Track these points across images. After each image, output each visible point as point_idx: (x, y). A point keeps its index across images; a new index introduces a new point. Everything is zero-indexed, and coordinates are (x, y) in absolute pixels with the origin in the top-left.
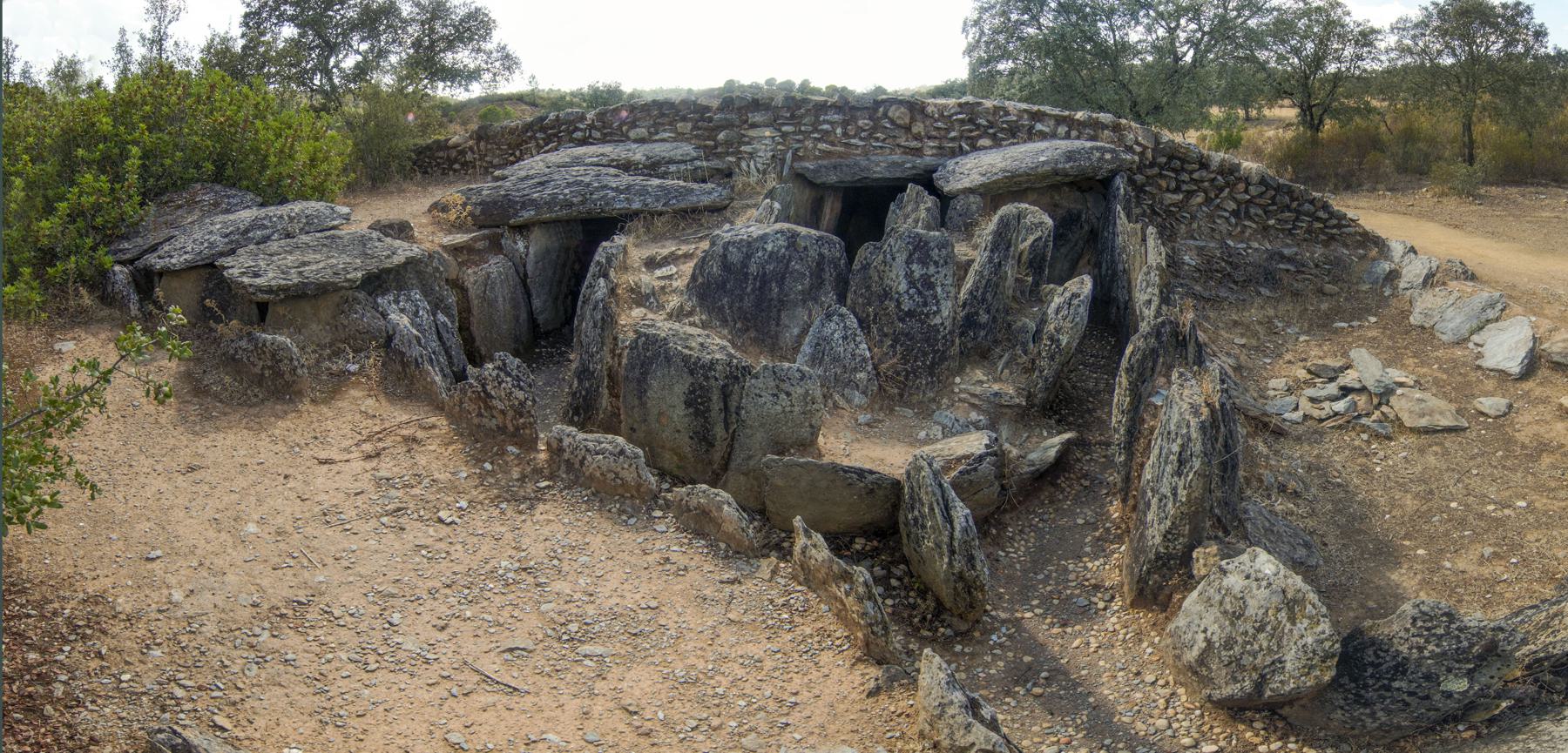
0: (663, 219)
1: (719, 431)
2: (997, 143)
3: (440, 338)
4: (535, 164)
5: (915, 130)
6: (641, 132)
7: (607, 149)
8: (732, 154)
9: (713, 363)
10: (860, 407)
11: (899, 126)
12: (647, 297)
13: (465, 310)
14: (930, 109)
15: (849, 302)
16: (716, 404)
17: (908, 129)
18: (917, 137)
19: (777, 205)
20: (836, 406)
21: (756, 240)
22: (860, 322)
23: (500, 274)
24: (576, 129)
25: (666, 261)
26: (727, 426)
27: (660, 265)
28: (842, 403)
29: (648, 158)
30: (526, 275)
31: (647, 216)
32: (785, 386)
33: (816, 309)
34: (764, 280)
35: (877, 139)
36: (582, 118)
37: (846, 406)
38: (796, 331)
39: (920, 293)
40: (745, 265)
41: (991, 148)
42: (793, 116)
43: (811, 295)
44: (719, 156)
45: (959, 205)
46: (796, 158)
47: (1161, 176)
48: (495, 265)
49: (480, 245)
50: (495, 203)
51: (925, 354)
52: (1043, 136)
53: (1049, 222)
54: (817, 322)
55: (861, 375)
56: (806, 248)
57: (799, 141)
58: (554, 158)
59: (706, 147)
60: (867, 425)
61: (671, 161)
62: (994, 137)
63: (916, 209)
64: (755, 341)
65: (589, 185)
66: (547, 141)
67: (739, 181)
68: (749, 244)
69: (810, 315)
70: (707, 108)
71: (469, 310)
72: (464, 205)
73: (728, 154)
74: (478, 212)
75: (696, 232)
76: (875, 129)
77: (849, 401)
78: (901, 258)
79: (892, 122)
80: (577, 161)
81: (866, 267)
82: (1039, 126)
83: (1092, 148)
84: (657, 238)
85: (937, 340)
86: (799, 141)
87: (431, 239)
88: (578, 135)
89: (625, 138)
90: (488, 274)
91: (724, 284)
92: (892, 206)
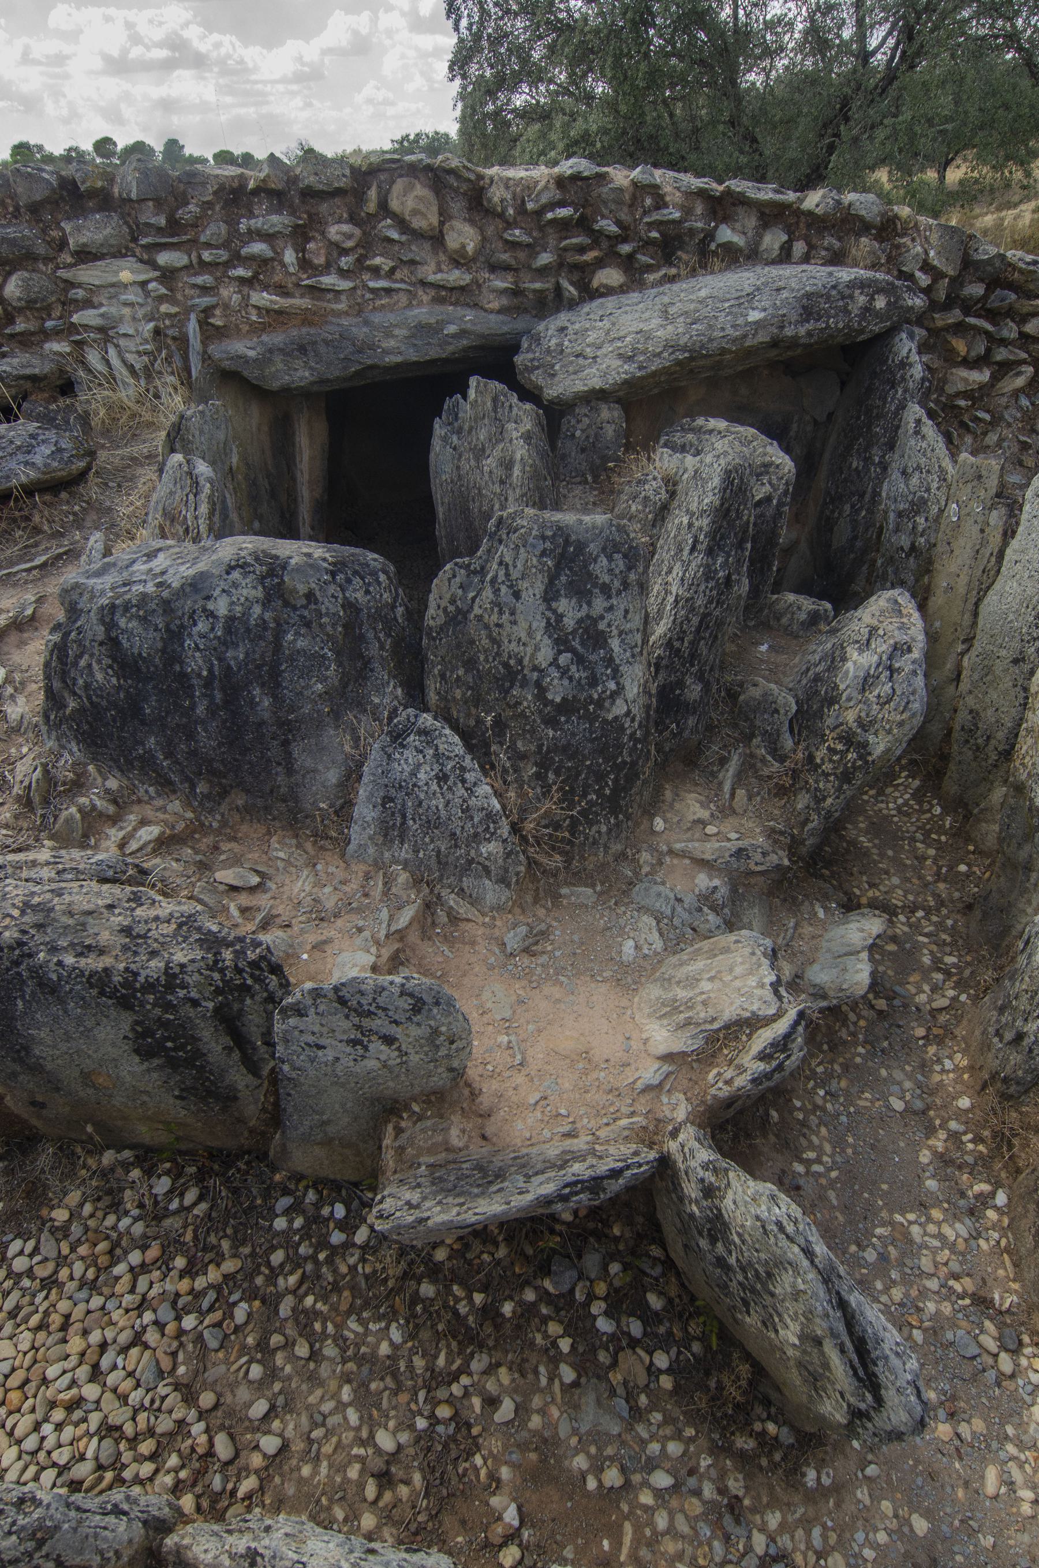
1: (239, 1078)
2: (635, 277)
5: (452, 242)
8: (56, 334)
9: (172, 978)
10: (499, 908)
11: (417, 235)
14: (497, 194)
15: (432, 697)
16: (213, 1043)
17: (437, 239)
18: (459, 259)
19: (202, 468)
20: (454, 919)
21: (181, 593)
22: (466, 736)
26: (252, 1066)
28: (463, 909)
32: (378, 1023)
33: (365, 725)
34: (230, 687)
35: (376, 271)
37: (472, 913)
38: (332, 776)
39: (580, 660)
41: (622, 290)
42: (174, 226)
43: (348, 696)
45: (579, 426)
46: (211, 333)
47: (960, 328)
51: (601, 777)
52: (733, 257)
53: (785, 463)
54: (375, 755)
55: (491, 848)
56: (310, 596)
57: (205, 290)
60: (526, 950)
62: (628, 264)
63: (499, 435)
64: (248, 812)
67: (94, 400)
68: (167, 606)
69: (356, 740)
73: (47, 335)
75: (26, 554)
76: (367, 245)
77: (475, 902)
78: (533, 590)
79: (402, 224)
81: (458, 617)
82: (726, 234)
83: (852, 285)
85: (620, 746)
86: (205, 290)
92: (439, 429)
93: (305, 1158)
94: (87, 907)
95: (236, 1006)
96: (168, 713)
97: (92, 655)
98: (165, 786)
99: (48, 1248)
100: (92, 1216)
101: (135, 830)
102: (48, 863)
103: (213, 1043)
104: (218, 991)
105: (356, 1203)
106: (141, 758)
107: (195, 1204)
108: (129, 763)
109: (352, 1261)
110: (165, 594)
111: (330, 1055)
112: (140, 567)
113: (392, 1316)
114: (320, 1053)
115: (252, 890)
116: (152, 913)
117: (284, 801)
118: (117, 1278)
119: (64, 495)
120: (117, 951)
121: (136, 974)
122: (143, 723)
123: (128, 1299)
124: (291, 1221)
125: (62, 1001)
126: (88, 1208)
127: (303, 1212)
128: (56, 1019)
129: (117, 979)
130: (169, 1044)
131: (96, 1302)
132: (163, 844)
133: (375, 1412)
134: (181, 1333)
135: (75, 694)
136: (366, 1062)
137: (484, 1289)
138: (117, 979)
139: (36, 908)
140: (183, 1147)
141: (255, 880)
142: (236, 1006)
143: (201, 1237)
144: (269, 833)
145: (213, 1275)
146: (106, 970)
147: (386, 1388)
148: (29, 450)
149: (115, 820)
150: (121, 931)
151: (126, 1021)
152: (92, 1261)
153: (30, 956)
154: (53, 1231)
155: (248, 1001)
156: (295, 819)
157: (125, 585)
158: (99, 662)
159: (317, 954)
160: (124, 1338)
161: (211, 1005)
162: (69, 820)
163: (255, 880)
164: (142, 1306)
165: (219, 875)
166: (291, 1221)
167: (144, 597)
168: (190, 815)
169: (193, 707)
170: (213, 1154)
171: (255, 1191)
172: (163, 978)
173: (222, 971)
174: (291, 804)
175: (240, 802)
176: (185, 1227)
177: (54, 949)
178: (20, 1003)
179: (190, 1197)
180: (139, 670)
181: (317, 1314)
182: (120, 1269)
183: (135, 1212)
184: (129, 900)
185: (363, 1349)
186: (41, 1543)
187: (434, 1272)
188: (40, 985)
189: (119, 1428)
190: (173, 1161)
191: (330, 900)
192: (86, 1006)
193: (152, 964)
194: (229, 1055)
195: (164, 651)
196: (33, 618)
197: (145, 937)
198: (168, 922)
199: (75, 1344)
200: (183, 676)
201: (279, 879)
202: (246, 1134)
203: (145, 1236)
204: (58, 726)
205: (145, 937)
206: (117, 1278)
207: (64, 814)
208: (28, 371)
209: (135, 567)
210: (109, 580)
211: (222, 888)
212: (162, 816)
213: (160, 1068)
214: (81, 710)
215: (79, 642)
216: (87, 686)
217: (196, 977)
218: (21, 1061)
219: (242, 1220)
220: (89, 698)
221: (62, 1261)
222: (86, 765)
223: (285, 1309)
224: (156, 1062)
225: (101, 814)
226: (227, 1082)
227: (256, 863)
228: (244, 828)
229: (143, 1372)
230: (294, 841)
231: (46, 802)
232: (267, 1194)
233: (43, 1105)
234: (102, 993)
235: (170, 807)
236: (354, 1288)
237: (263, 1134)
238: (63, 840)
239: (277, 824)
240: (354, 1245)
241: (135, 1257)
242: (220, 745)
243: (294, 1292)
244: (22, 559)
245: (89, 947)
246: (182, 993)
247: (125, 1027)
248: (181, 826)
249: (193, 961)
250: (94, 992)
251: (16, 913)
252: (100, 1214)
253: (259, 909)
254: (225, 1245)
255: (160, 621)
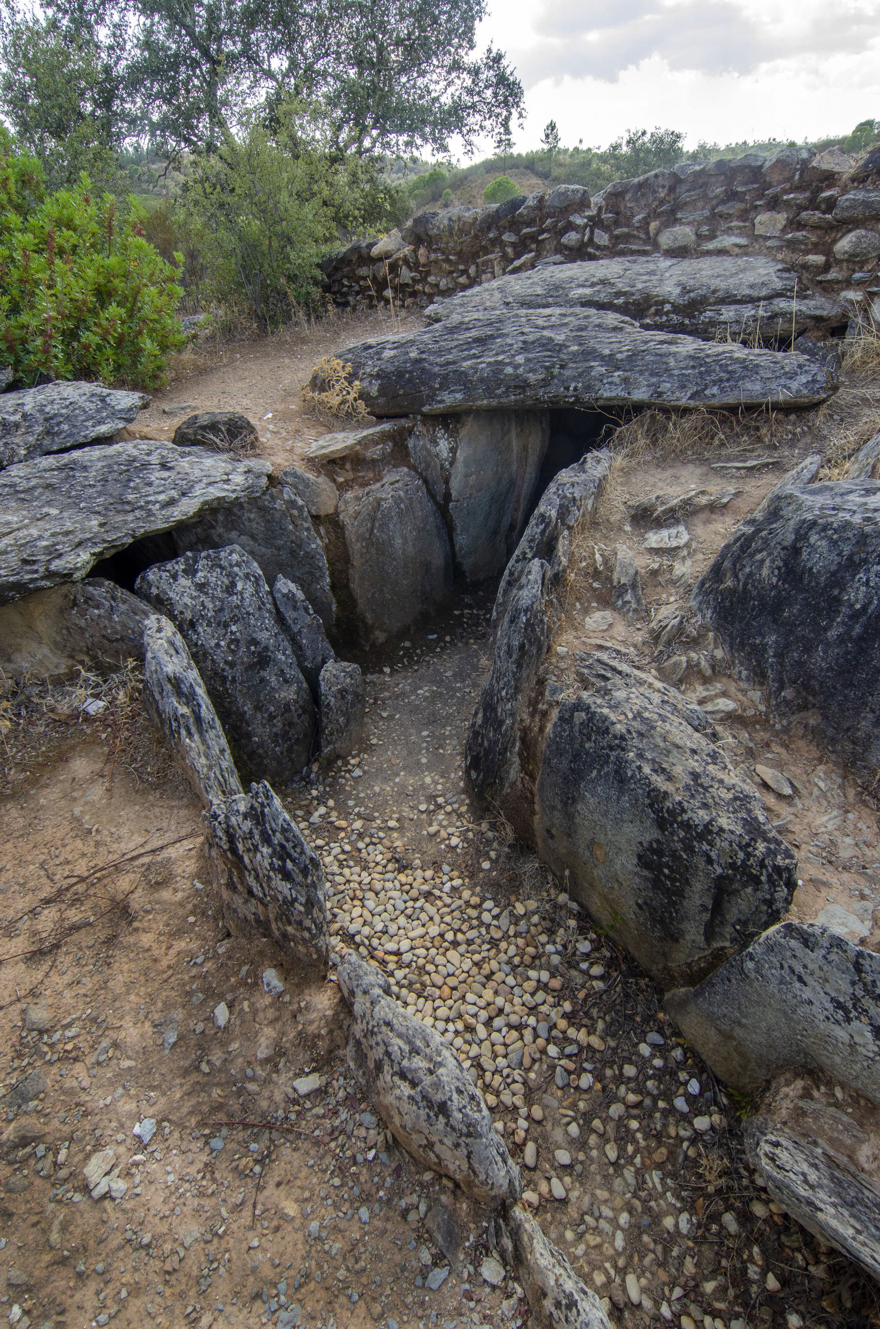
0: (687, 423)
1: (693, 932)
3: (280, 618)
4: (487, 298)
6: (683, 233)
7: (608, 268)
9: (708, 832)
12: (622, 590)
13: (340, 558)
16: (698, 895)
23: (398, 501)
24: (571, 227)
25: (672, 517)
27: (659, 524)
29: (685, 290)
30: (448, 496)
31: (657, 414)
36: (583, 204)
40: (838, 579)
44: (829, 288)
48: (392, 486)
49: (374, 452)
50: (400, 374)
58: (519, 285)
59: (805, 267)
61: (729, 299)
64: (815, 735)
65: (562, 346)
66: (521, 248)
68: (863, 539)
70: (829, 178)
71: (346, 559)
72: (351, 378)
73: (848, 283)
74: (374, 391)
80: (556, 295)
84: (669, 458)
87: (289, 446)
88: (571, 238)
89: (650, 246)
90: (379, 501)
91: (778, 606)
93: (693, 1024)
94: (679, 742)
95: (736, 886)
96: (802, 623)
97: (769, 554)
98: (759, 676)
99: (504, 921)
100: (535, 925)
101: (716, 696)
102: (659, 691)
103: (698, 895)
104: (733, 866)
105: (708, 1095)
106: (754, 646)
107: (596, 978)
108: (742, 645)
109: (682, 1133)
110: (867, 529)
111: (807, 994)
112: (854, 498)
113: (692, 1209)
114: (798, 985)
115: (780, 796)
116: (721, 775)
117: (854, 743)
118: (528, 979)
119: (793, 417)
120: (680, 786)
121: (684, 811)
122: (775, 621)
123: (527, 997)
124: (653, 1056)
125: (621, 792)
126: (535, 919)
127: (666, 1059)
128: (608, 799)
129: (668, 804)
130: (666, 871)
131: (510, 980)
132: (732, 719)
133: (636, 1259)
134: (543, 1052)
135: (736, 576)
136: (836, 1028)
137: (784, 1282)
138: (668, 804)
139: (644, 720)
140: (612, 934)
141: (788, 791)
142: (736, 886)
143: (589, 1004)
144: (820, 761)
145: (582, 1036)
146: (666, 793)
147: (654, 1252)
148: (792, 376)
149: (706, 681)
150: (692, 773)
151: (651, 834)
152: (521, 954)
153: (623, 749)
154: (511, 914)
155: (749, 890)
156: (853, 763)
157: (834, 509)
158: (773, 561)
159: (811, 888)
160: (514, 1019)
161: (719, 871)
162: (676, 665)
163: (788, 791)
164: (533, 1010)
165: (760, 768)
166: (653, 1056)
167: (846, 525)
168: (762, 708)
169: (826, 629)
170: (629, 959)
171: (639, 1009)
172: (700, 828)
173: (748, 855)
174: (859, 750)
175: (812, 722)
176: (583, 986)
177: (640, 756)
178: (595, 773)
179: (597, 970)
180: (801, 580)
181: (634, 1141)
182: (533, 974)
183: (560, 948)
184: (708, 755)
185: (652, 1203)
186: (469, 1135)
187: (745, 1217)
188: (616, 772)
189: (484, 1071)
190: (599, 936)
191: (846, 849)
192: (635, 805)
193: (701, 812)
194: (701, 912)
195: (833, 574)
196: (725, 506)
197: (706, 789)
198: (729, 790)
199: (488, 994)
200: (837, 600)
201: (807, 802)
202: (660, 966)
203: (556, 967)
204: (707, 593)
205: (706, 789)
206: (528, 979)
207: (675, 659)
208: (818, 313)
209: (851, 497)
210: (820, 500)
211: (757, 779)
212: (740, 697)
213: (646, 879)
214: (732, 591)
215: (766, 541)
216: (751, 575)
217: (725, 845)
218: (565, 804)
219: (623, 1025)
220: (745, 584)
221: (506, 937)
222: (709, 630)
223: (616, 1110)
224: (646, 873)
225: (700, 672)
226: (682, 926)
227: (795, 777)
228: (801, 743)
229: (513, 1051)
230: (839, 780)
231: (669, 643)
232: (649, 1018)
233: (552, 837)
234: (651, 806)
235: (750, 694)
236: (672, 1154)
237: (673, 978)
238: (663, 675)
239: (833, 757)
240: (691, 1124)
241: (545, 976)
242: (830, 669)
243: (628, 1107)
244: (736, 459)
245: (664, 770)
246: (705, 847)
247: (647, 838)
248: (750, 712)
249: (732, 832)
250: (647, 801)
251: (630, 715)
252: (540, 928)
253: (778, 816)
254: (600, 1025)
255: (847, 549)
